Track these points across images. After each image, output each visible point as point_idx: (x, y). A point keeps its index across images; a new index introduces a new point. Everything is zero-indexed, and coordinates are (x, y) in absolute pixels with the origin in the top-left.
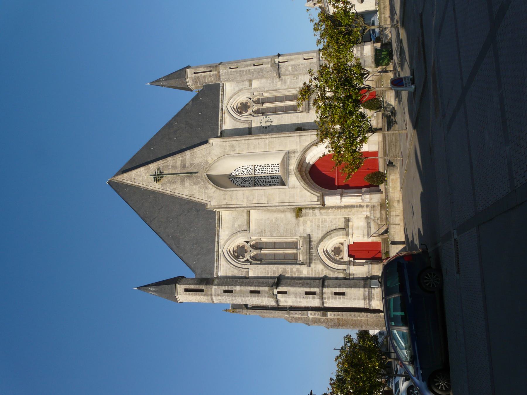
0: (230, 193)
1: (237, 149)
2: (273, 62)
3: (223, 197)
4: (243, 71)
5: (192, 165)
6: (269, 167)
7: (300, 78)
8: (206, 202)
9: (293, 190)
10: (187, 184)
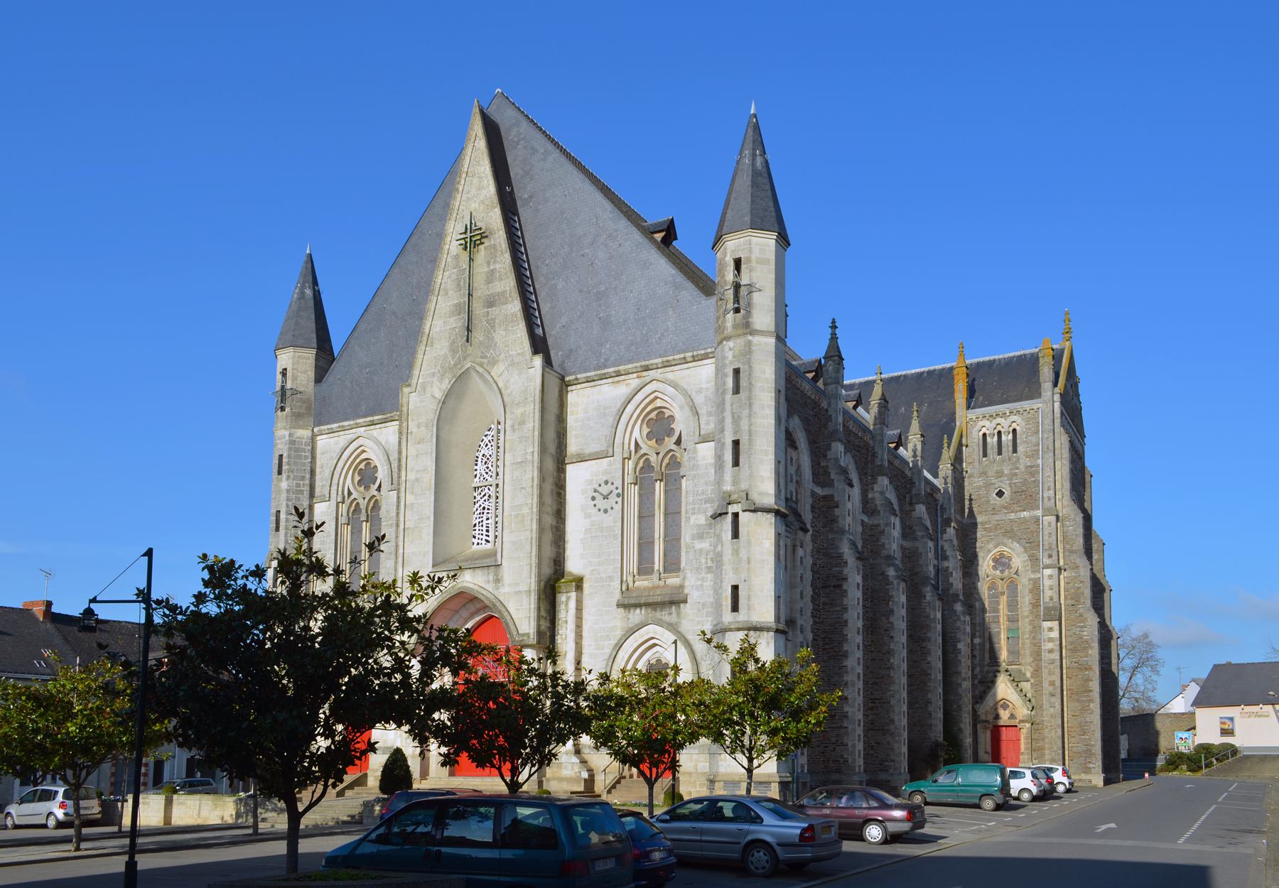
2: (734, 497)
3: (423, 420)
5: (491, 324)
7: (710, 576)
8: (414, 382)
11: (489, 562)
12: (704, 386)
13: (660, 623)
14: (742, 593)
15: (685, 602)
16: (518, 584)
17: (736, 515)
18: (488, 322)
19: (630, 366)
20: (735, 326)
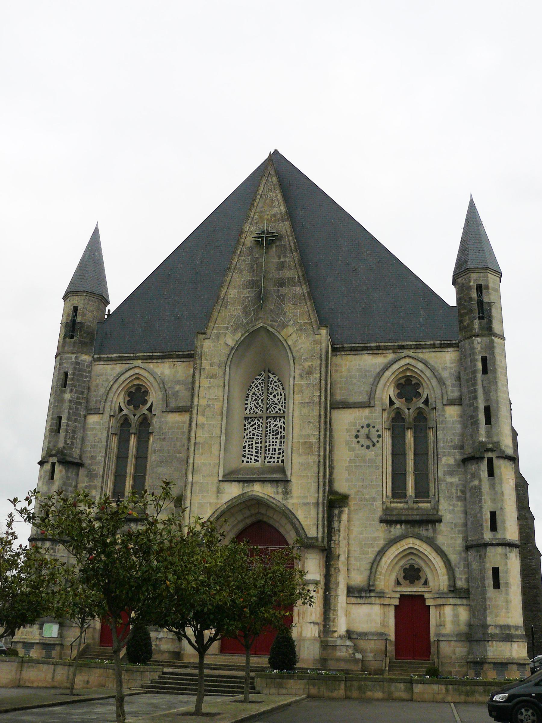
0: (221, 373)
1: (304, 382)
3: (216, 361)
4: (475, 384)
6: (278, 444)
7: (459, 503)
9: (215, 489)
10: (246, 293)
11: (278, 476)
12: (448, 365)
13: (419, 537)
14: (498, 518)
15: (440, 521)
16: (306, 497)
17: (53, 465)
18: (278, 296)
19: (390, 344)
20: (481, 328)
